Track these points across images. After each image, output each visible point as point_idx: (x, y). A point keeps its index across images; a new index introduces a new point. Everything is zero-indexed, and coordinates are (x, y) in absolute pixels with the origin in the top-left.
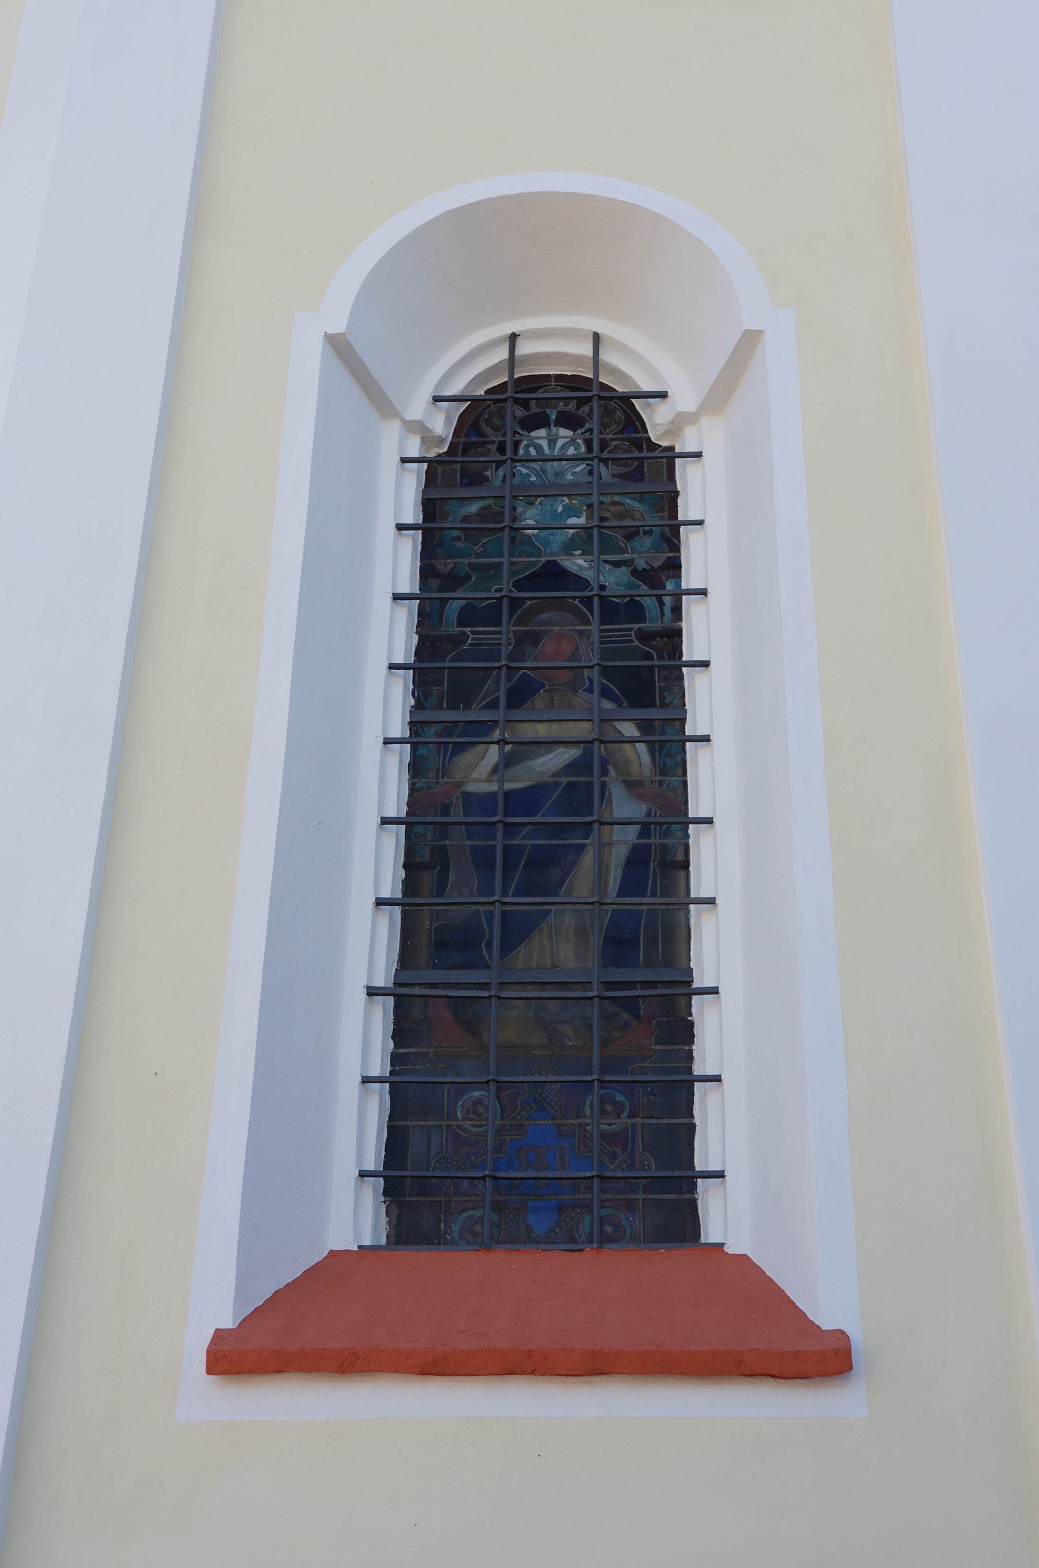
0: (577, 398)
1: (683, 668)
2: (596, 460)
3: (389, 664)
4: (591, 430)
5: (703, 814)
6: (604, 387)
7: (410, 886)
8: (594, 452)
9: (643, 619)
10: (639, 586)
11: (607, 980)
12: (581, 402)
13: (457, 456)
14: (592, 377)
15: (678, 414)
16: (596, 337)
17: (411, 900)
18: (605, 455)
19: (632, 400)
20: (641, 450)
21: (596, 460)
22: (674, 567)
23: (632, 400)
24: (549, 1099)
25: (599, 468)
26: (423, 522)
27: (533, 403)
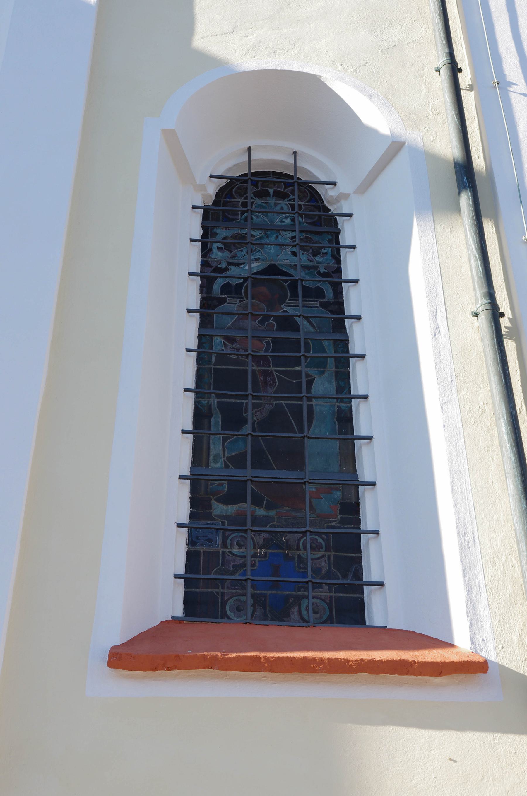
0: (285, 183)
1: (345, 319)
2: (297, 214)
3: (180, 475)
4: (293, 200)
5: (361, 393)
6: (299, 179)
7: (200, 344)
8: (295, 210)
9: (324, 297)
10: (320, 285)
11: (335, 339)
12: (287, 185)
13: (220, 206)
14: (294, 175)
15: (341, 193)
16: (295, 153)
17: (201, 350)
18: (301, 212)
19: (295, 318)
20: (320, 211)
21: (297, 214)
22: (339, 271)
23: (295, 318)
24: (279, 539)
25: (298, 218)
26: (202, 238)
27: (259, 184)
